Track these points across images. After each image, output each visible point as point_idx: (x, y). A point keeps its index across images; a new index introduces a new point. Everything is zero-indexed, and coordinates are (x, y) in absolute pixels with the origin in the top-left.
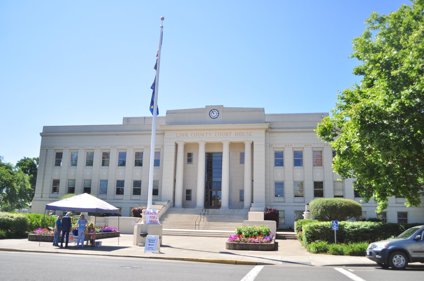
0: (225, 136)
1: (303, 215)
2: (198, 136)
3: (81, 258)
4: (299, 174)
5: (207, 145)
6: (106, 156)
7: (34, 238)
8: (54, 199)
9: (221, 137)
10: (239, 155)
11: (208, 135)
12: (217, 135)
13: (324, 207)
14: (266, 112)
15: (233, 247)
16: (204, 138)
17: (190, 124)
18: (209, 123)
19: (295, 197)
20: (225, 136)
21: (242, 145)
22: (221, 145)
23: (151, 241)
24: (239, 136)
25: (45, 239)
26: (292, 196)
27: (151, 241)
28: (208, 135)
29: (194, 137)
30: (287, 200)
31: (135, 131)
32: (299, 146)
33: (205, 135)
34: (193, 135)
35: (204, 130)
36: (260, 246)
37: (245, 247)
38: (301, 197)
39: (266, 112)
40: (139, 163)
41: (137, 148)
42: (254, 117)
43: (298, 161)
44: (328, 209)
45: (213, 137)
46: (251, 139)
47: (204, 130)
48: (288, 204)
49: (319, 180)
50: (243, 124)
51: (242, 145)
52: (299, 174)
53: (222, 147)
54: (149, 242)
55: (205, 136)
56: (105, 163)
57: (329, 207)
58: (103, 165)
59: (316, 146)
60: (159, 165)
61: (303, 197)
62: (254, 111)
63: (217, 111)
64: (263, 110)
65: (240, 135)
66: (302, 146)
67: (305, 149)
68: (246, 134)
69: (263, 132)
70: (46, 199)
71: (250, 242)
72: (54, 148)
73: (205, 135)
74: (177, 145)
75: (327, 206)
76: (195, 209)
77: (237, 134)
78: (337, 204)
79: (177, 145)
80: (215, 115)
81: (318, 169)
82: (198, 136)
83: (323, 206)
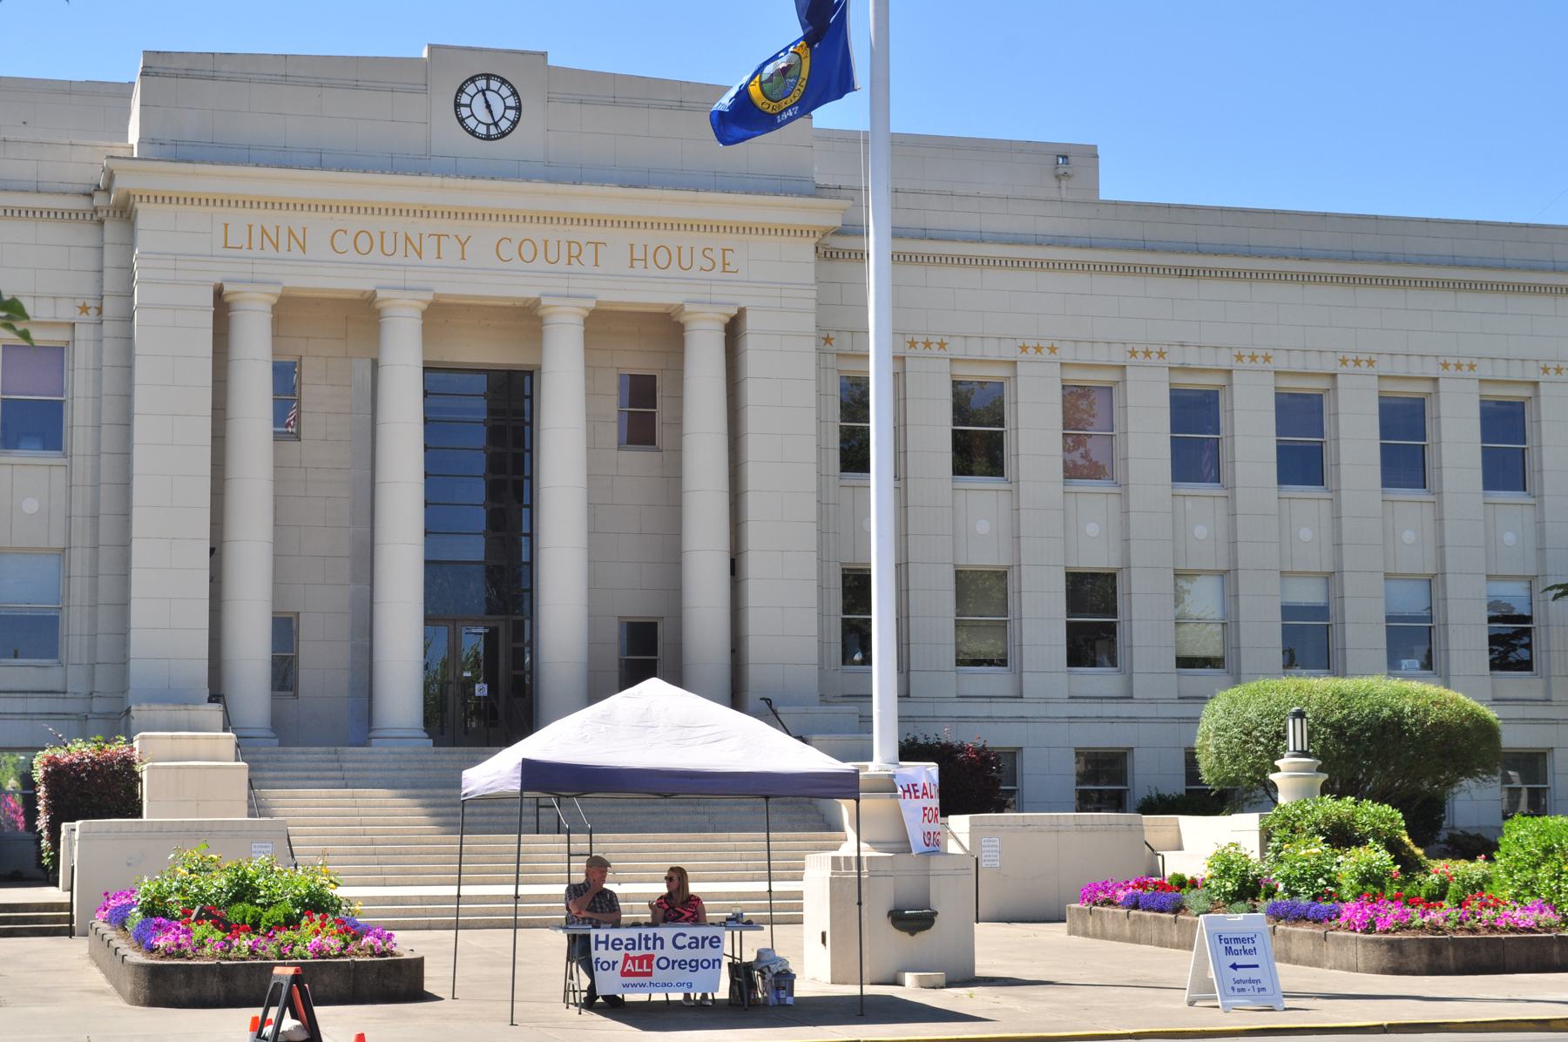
0: (562, 265)
1: (1273, 777)
2: (376, 254)
4: (983, 527)
6: (1086, 410)
7: (214, 986)
10: (614, 391)
11: (450, 247)
12: (508, 250)
13: (1339, 729)
15: (1425, 957)
17: (321, 166)
18: (453, 168)
20: (562, 265)
21: (668, 329)
22: (528, 319)
23: (1235, 946)
24: (653, 270)
27: (1235, 946)
28: (450, 247)
29: (352, 255)
30: (1140, 687)
32: (1101, 355)
33: (429, 246)
34: (343, 242)
35: (425, 212)
36: (1556, 949)
37: (1484, 956)
38: (991, 663)
41: (1501, 375)
44: (1354, 739)
45: (487, 264)
46: (730, 298)
47: (425, 212)
48: (1041, 710)
49: (1094, 560)
50: (690, 195)
51: (668, 329)
52: (978, 521)
53: (541, 332)
54: (1229, 951)
56: (1302, 463)
57: (1362, 731)
59: (1084, 355)
60: (995, 467)
61: (1003, 662)
63: (505, 91)
65: (662, 258)
66: (1009, 351)
67: (1236, 376)
68: (700, 261)
69: (806, 249)
71: (1493, 929)
72: (1271, 366)
73: (429, 246)
74: (222, 307)
75: (1351, 723)
76: (377, 751)
77: (639, 253)
78: (1398, 714)
79: (222, 307)
81: (1093, 497)
82: (376, 254)
83: (1331, 726)
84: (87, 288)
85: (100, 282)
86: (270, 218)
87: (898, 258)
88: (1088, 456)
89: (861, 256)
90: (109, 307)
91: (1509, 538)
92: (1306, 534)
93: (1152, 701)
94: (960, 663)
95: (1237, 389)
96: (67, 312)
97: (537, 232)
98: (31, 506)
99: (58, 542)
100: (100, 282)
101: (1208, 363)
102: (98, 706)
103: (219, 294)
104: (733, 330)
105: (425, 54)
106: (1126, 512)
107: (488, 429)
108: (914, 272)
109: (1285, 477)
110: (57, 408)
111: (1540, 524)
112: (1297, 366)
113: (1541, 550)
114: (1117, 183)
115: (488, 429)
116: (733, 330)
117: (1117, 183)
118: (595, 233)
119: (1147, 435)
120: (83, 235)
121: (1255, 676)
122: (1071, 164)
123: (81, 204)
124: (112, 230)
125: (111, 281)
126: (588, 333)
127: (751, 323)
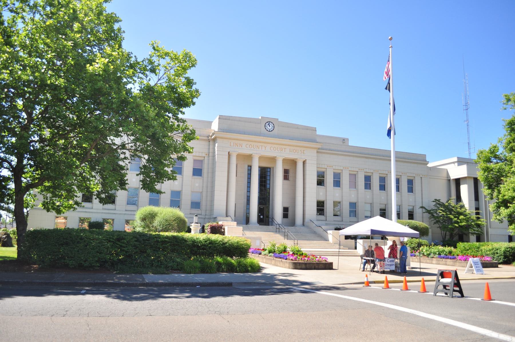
3: (504, 283)
5: (261, 158)
8: (351, 223)
9: (279, 152)
11: (264, 148)
12: (272, 149)
14: (318, 133)
16: (261, 151)
18: (264, 135)
19: (127, 204)
21: (294, 163)
22: (273, 159)
25: (317, 267)
26: (125, 203)
28: (264, 148)
31: (326, 149)
35: (260, 142)
39: (318, 133)
40: (383, 187)
42: (307, 136)
43: (337, 183)
45: (269, 152)
46: (304, 158)
51: (294, 163)
55: (260, 148)
58: (366, 188)
62: (307, 129)
64: (315, 130)
68: (300, 152)
69: (315, 151)
70: (98, 211)
80: (270, 128)
84: (207, 151)
85: (209, 151)
86: (237, 142)
87: (396, 161)
88: (353, 184)
89: (390, 160)
90: (211, 154)
91: (411, 200)
92: (337, 195)
93: (97, 209)
94: (127, 204)
95: (343, 173)
96: (204, 155)
97: (276, 146)
98: (197, 185)
99: (201, 191)
100: (209, 151)
101: (369, 171)
102: (207, 217)
103: (229, 153)
104: (304, 163)
105: (260, 118)
106: (358, 193)
107: (265, 175)
108: (320, 155)
109: (380, 189)
110: (201, 170)
111: (415, 198)
112: (337, 168)
113: (415, 202)
114: (351, 143)
115: (265, 175)
116: (304, 163)
117: (351, 143)
118: (285, 147)
119: (361, 182)
120: (207, 143)
121: (143, 206)
122: (344, 141)
123: (207, 138)
124: (211, 143)
125: (211, 150)
126: (237, 158)
127: (307, 162)
